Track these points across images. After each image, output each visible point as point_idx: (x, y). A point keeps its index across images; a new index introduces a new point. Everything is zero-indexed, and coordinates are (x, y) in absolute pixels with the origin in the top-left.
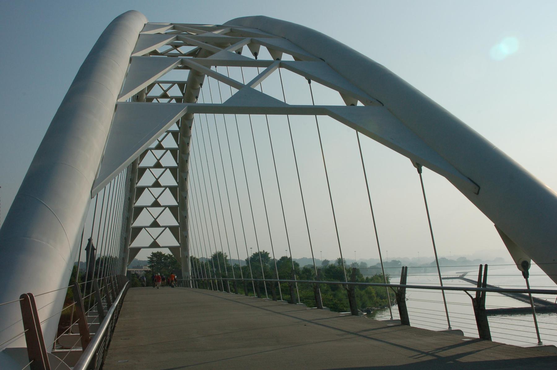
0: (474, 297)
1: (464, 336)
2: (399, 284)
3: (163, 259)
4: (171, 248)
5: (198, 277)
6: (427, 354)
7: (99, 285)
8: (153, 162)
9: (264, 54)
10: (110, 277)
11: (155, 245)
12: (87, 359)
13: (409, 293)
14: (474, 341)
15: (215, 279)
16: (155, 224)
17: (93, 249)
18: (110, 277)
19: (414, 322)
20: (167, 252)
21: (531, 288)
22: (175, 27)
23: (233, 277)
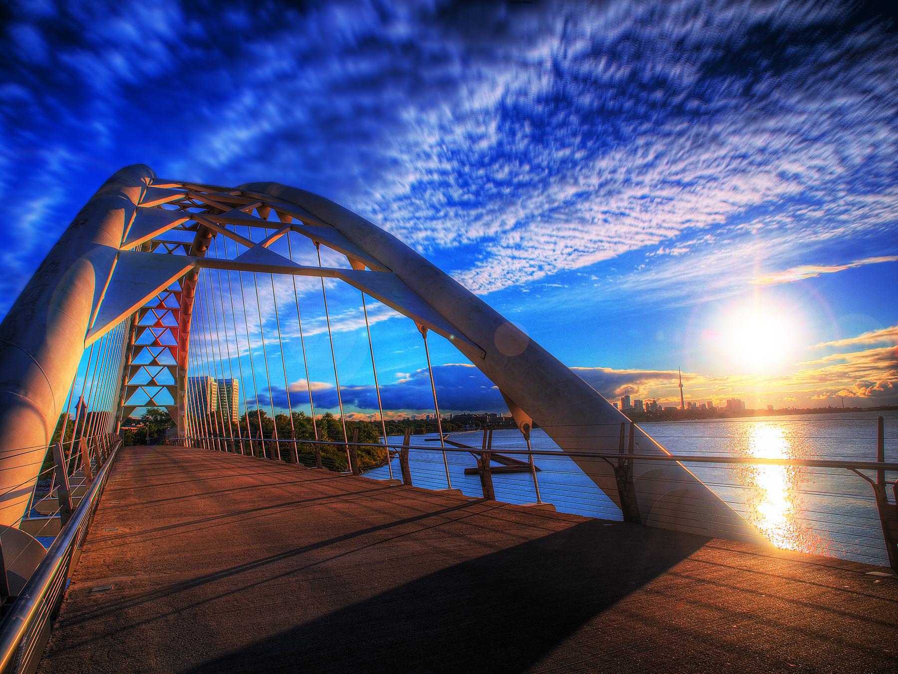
0: (616, 465)
1: (414, 485)
2: (402, 445)
3: (642, 267)
4: (166, 407)
5: (194, 436)
6: (523, 538)
7: (88, 445)
8: (152, 322)
9: (273, 217)
10: (102, 436)
11: (151, 403)
12: (17, 622)
13: (412, 454)
14: (478, 502)
15: (249, 440)
16: (152, 383)
17: (84, 407)
18: (102, 436)
19: (416, 484)
20: (163, 410)
21: (886, 461)
22: (184, 184)
23: (345, 440)
